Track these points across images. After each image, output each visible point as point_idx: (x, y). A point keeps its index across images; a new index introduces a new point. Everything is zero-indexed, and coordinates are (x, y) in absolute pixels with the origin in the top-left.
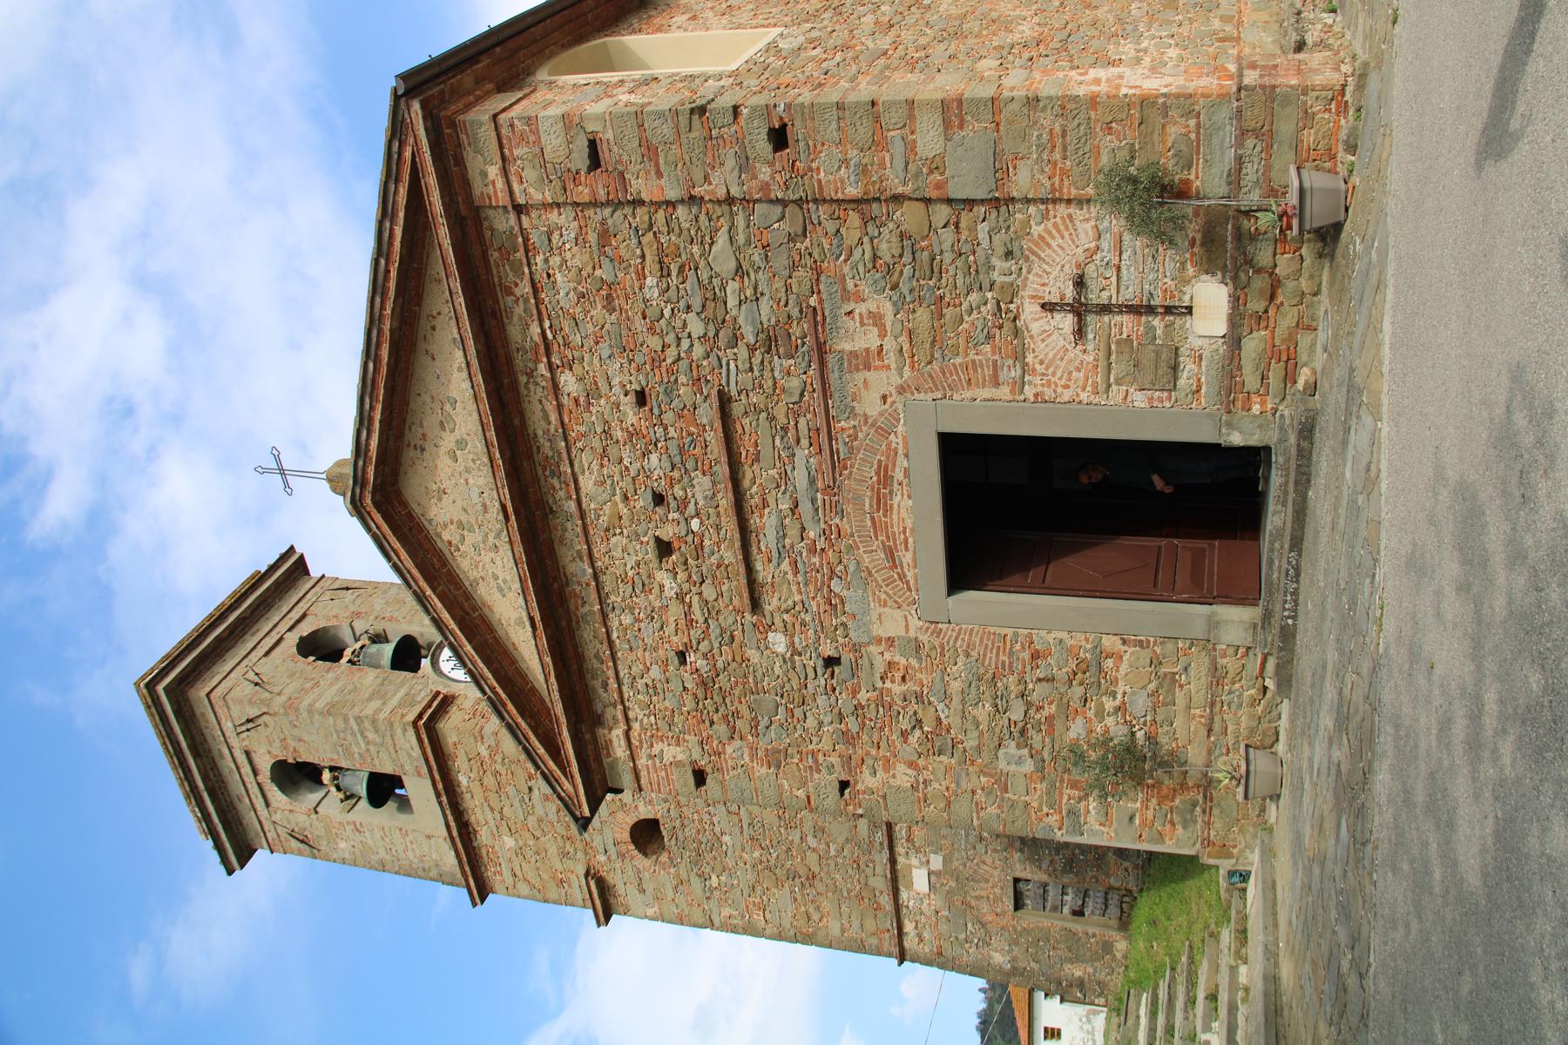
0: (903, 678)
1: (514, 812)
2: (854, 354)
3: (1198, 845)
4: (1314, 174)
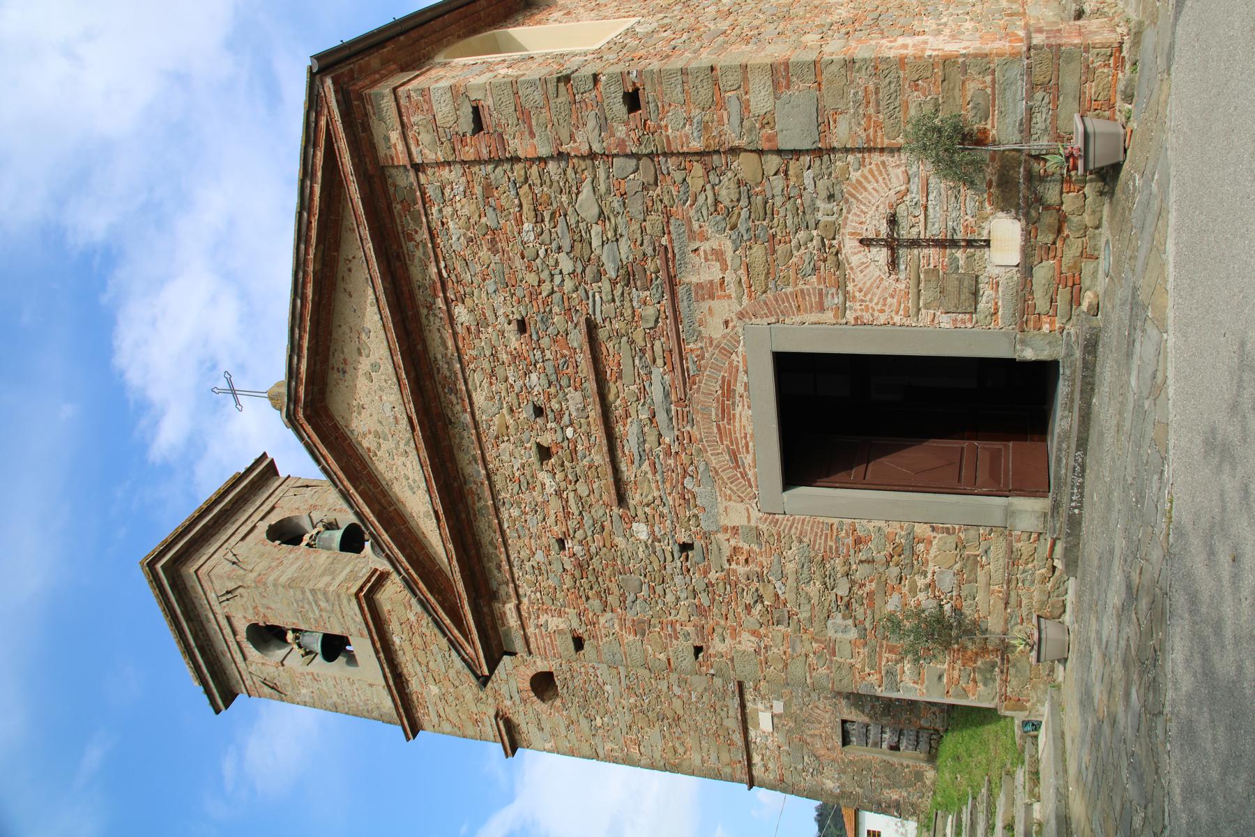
0: (747, 561)
1: (437, 665)
3: (997, 700)
4: (1095, 120)
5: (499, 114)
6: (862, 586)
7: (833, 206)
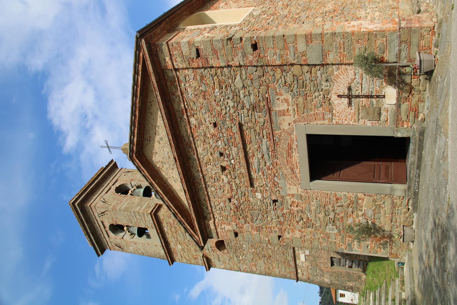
0: (297, 206)
1: (181, 238)
2: (280, 111)
3: (388, 254)
4: (424, 54)
5: (206, 51)
6: (339, 215)
7: (328, 84)
